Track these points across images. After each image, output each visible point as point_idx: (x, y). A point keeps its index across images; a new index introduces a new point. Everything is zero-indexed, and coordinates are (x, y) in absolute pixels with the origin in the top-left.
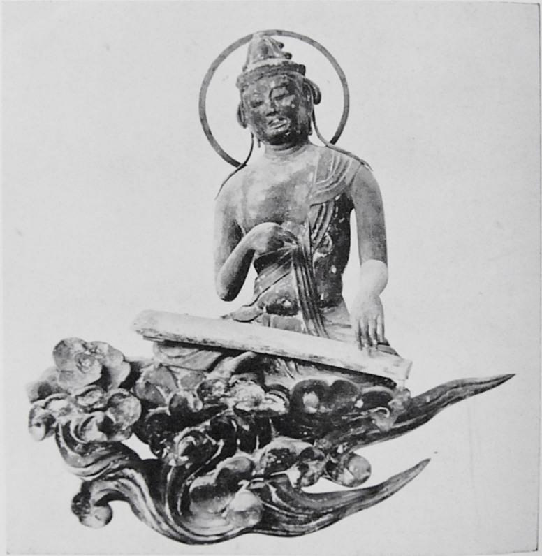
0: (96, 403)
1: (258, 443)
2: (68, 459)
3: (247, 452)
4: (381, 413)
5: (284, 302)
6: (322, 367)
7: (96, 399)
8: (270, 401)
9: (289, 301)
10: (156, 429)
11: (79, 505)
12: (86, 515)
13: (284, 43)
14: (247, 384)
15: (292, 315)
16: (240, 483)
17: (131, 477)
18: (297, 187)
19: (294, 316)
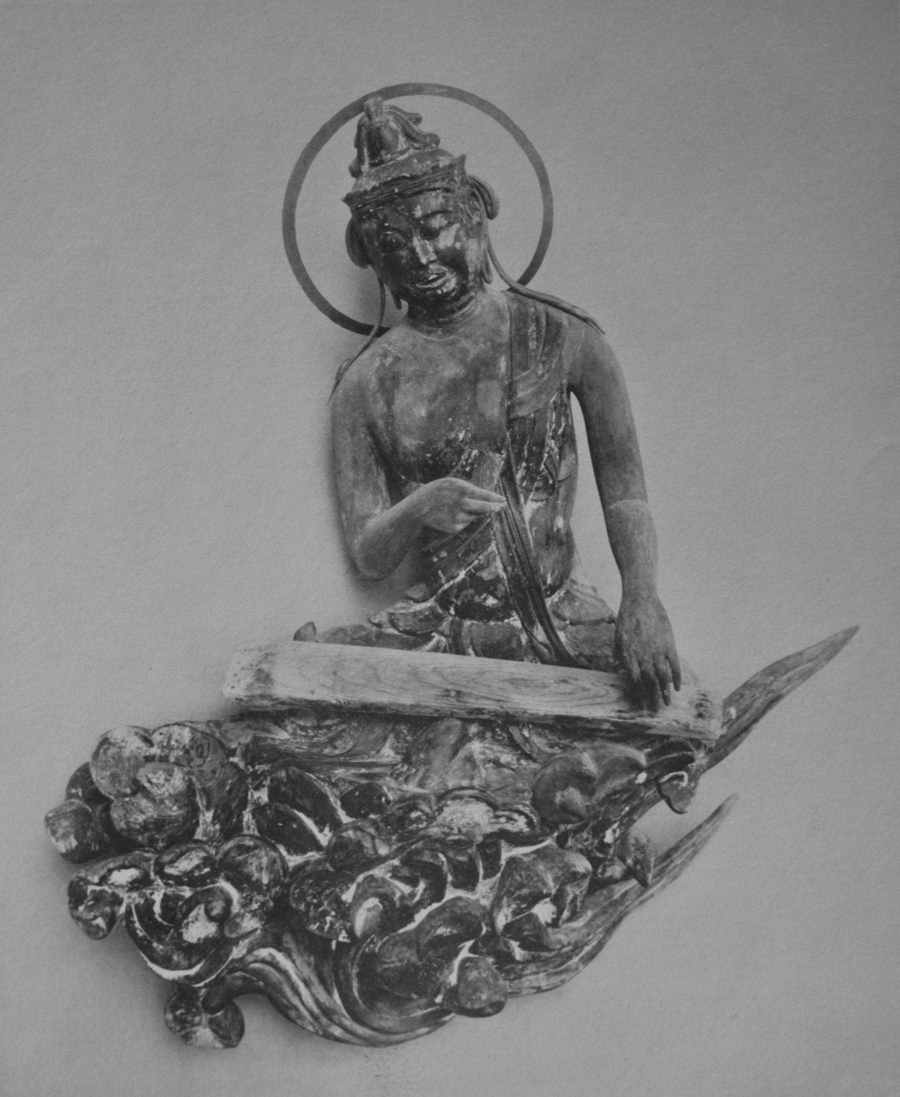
0: (198, 867)
1: (481, 872)
2: (75, 913)
3: (467, 889)
4: (675, 782)
5: (485, 599)
6: (383, 304)
7: (196, 862)
8: (503, 820)
9: (495, 597)
10: (311, 891)
11: (182, 1014)
12: (195, 1028)
13: (423, 115)
14: (462, 802)
15: (502, 619)
16: (327, 829)
17: (268, 959)
18: (480, 386)
19: (506, 621)
